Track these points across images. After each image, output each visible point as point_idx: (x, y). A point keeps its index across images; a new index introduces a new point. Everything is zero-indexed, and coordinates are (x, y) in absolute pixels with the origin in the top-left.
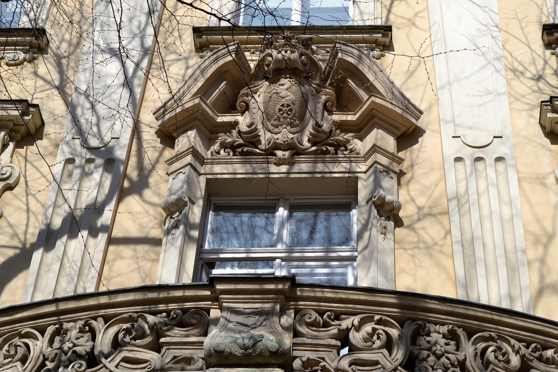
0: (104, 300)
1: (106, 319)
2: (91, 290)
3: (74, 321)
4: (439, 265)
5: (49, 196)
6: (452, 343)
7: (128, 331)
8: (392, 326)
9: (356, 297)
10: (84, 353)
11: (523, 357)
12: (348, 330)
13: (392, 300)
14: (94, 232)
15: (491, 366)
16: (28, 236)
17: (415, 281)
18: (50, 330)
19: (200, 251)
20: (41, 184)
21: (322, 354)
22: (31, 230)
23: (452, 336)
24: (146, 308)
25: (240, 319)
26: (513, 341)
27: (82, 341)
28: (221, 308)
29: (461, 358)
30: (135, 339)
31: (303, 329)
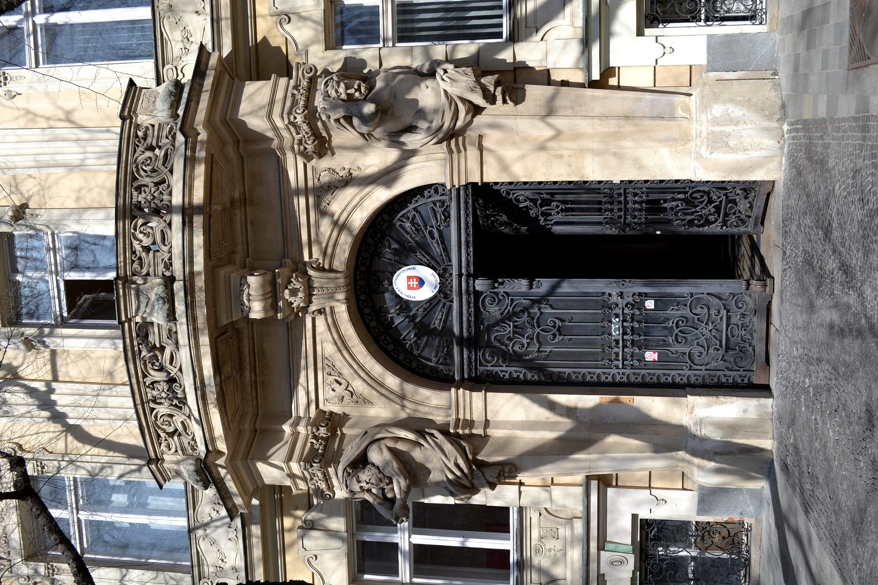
0: (134, 380)
1: (145, 376)
2: (128, 388)
3: (147, 393)
4: (56, 182)
5: (26, 421)
6: (143, 189)
7: (153, 364)
8: (136, 223)
9: (122, 243)
10: (168, 386)
11: (146, 149)
12: (142, 247)
13: (121, 224)
14: (51, 391)
15: (155, 168)
16: (57, 430)
17: (69, 197)
18: (152, 405)
19: (57, 326)
20: (17, 427)
21: (160, 260)
22: (52, 429)
23: (139, 189)
24: (137, 357)
25: (143, 306)
26: (136, 155)
27: (160, 388)
28: (137, 315)
29: (153, 185)
30: (158, 360)
31: (144, 271)
